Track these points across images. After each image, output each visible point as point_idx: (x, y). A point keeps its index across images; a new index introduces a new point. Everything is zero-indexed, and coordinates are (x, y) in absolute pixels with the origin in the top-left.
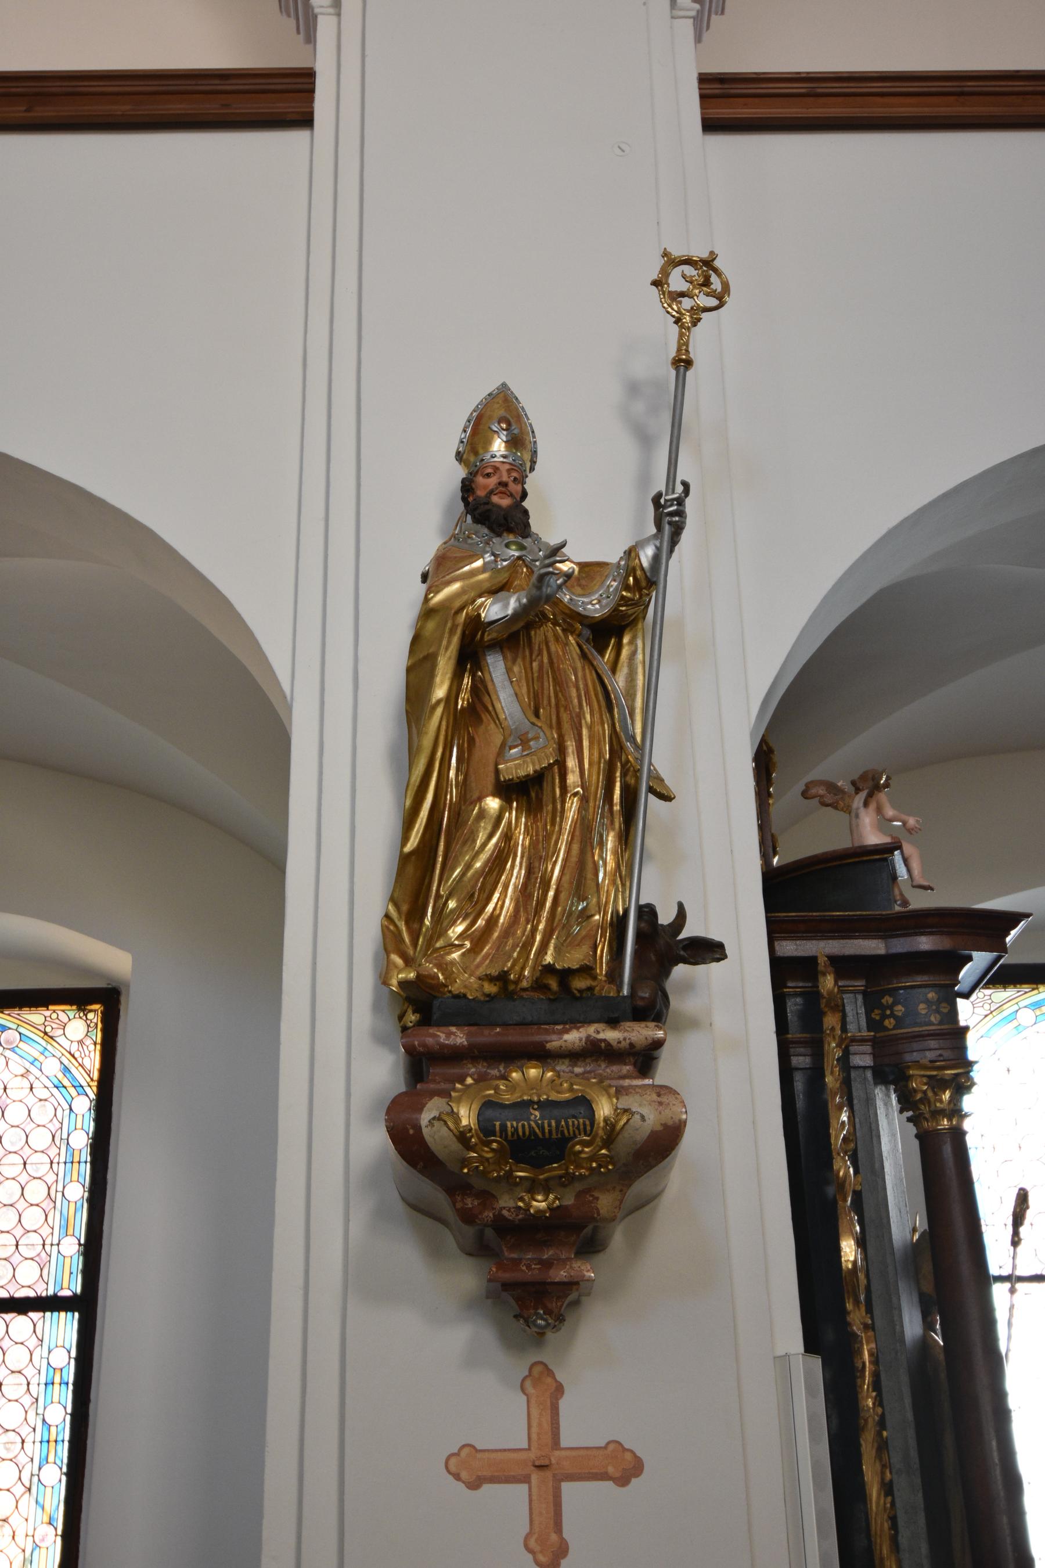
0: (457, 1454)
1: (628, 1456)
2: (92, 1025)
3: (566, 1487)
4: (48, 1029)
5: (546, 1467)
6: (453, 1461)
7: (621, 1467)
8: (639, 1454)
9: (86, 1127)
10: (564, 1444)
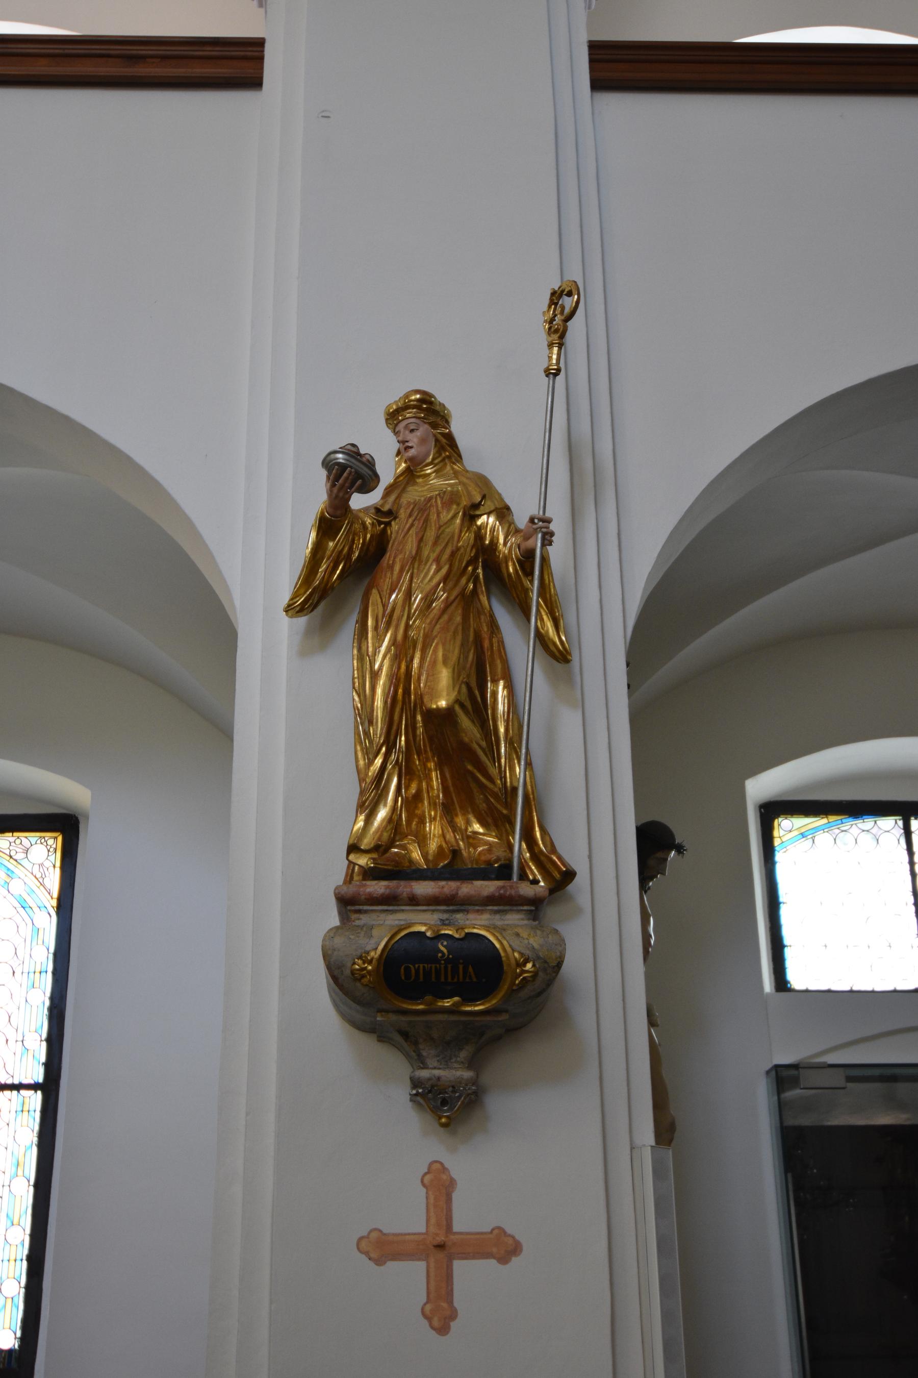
0: (367, 1237)
1: (510, 1241)
2: (52, 850)
4: (13, 853)
5: (442, 1249)
7: (501, 1247)
8: (517, 1237)
9: (31, 1125)
10: (456, 1228)
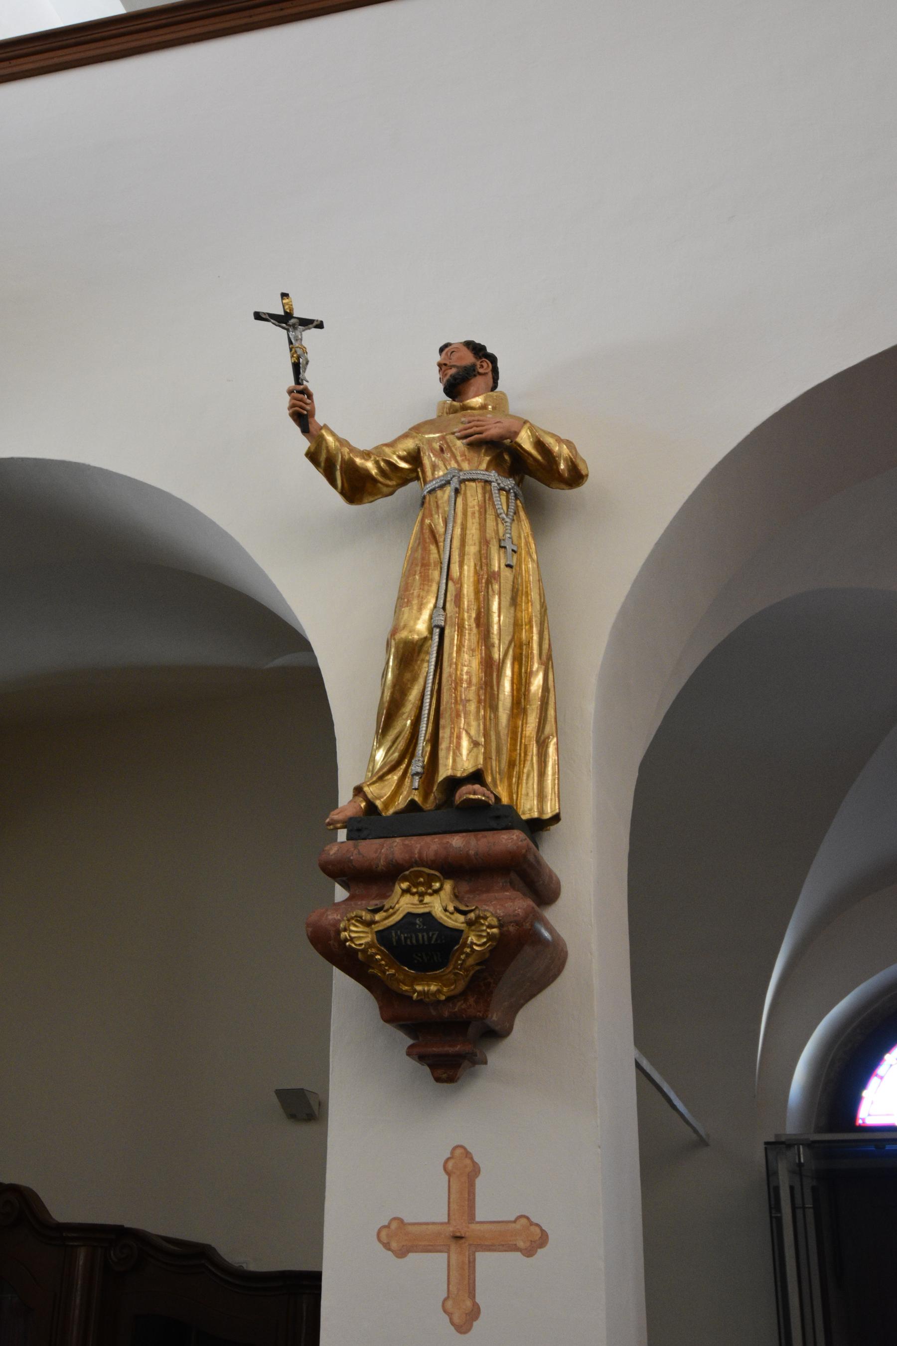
0: (387, 1227)
3: (484, 1260)
6: (384, 1233)
10: (479, 1217)
